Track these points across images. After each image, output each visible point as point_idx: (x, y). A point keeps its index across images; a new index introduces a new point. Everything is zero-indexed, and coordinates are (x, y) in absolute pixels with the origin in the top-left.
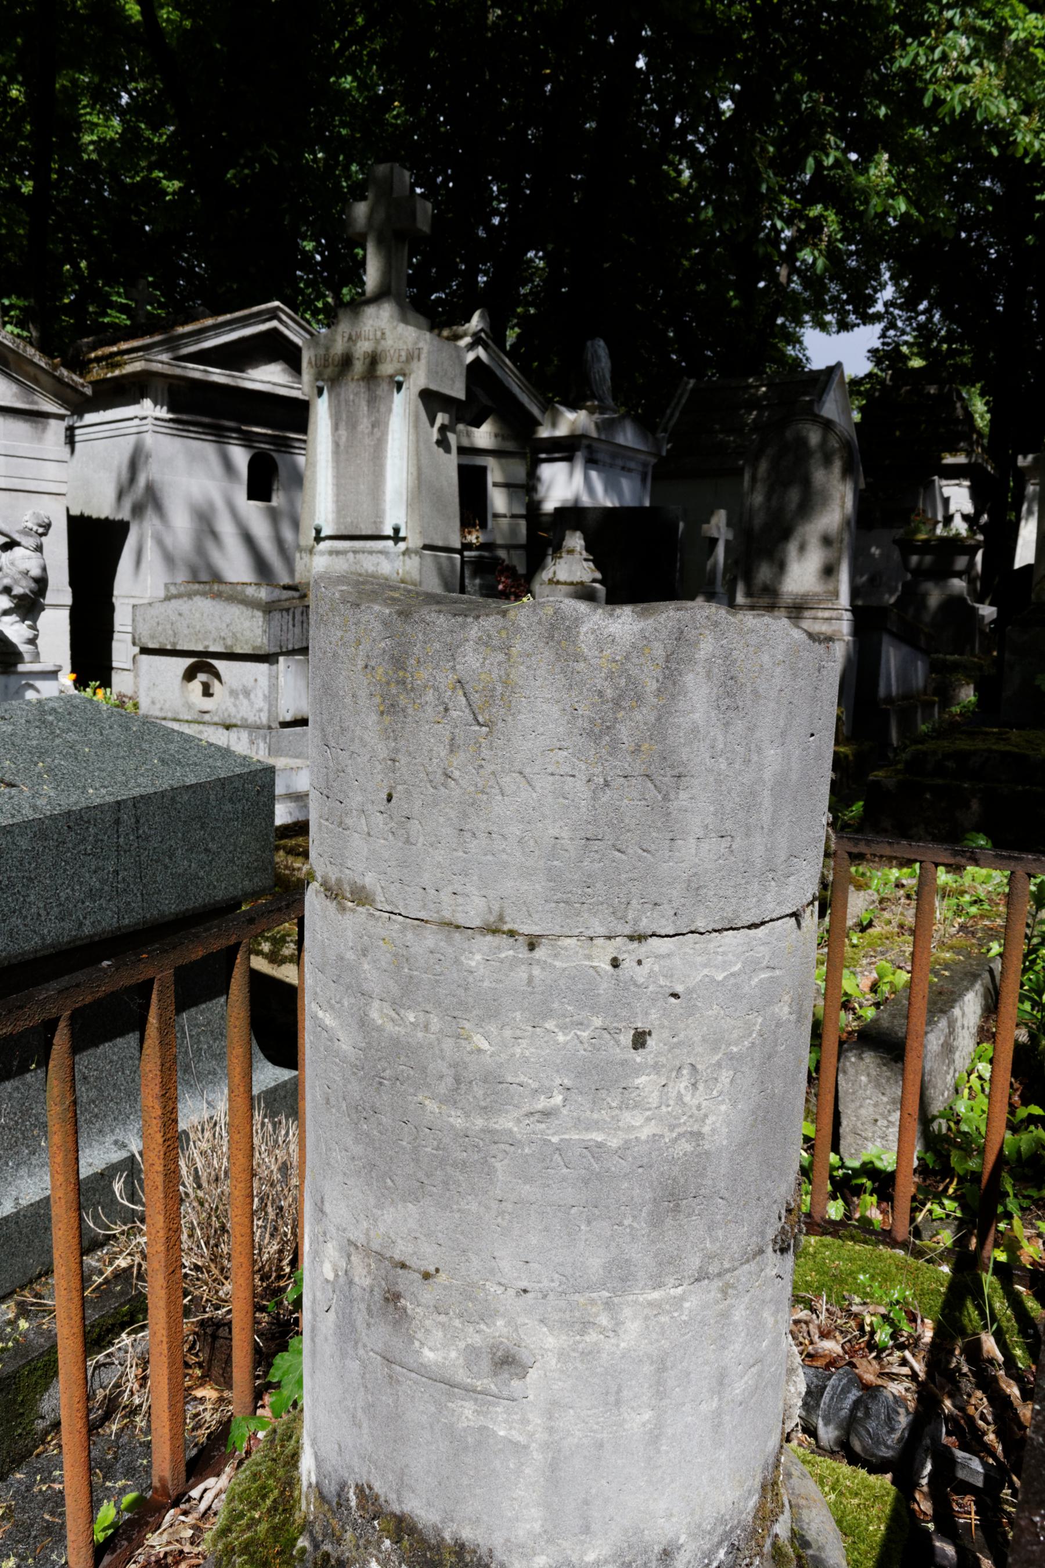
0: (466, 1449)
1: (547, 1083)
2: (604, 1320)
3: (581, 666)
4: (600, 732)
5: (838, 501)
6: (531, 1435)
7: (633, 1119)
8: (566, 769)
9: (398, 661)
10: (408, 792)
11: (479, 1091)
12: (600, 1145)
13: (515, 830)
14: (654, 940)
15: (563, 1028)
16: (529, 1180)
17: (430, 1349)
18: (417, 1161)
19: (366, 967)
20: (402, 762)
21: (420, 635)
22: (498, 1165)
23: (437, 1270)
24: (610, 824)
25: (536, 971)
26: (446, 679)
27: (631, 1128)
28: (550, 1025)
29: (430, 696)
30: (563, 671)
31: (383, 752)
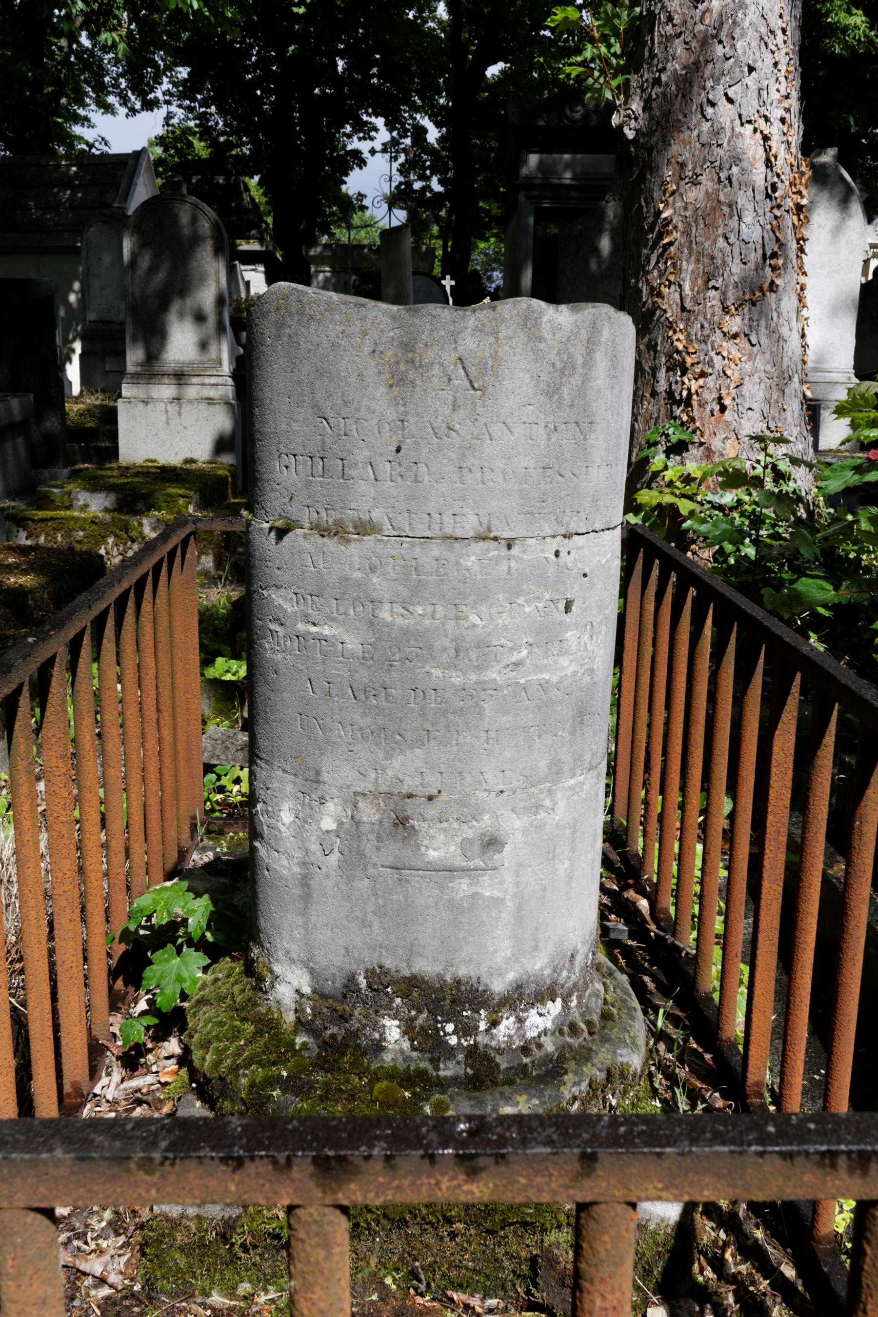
0: (463, 912)
1: (518, 642)
2: (547, 803)
3: (542, 346)
4: (552, 392)
5: (213, 277)
6: (506, 890)
7: (564, 661)
8: (533, 419)
9: (407, 345)
10: (416, 443)
11: (473, 655)
12: (547, 682)
13: (500, 464)
14: (575, 537)
15: (528, 602)
16: (505, 712)
17: (435, 849)
18: (423, 716)
19: (375, 580)
20: (411, 421)
21: (428, 326)
22: (486, 706)
23: (439, 792)
24: (557, 458)
25: (513, 564)
26: (449, 357)
27: (563, 668)
28: (521, 601)
29: (436, 370)
30: (532, 350)
31: (391, 414)
